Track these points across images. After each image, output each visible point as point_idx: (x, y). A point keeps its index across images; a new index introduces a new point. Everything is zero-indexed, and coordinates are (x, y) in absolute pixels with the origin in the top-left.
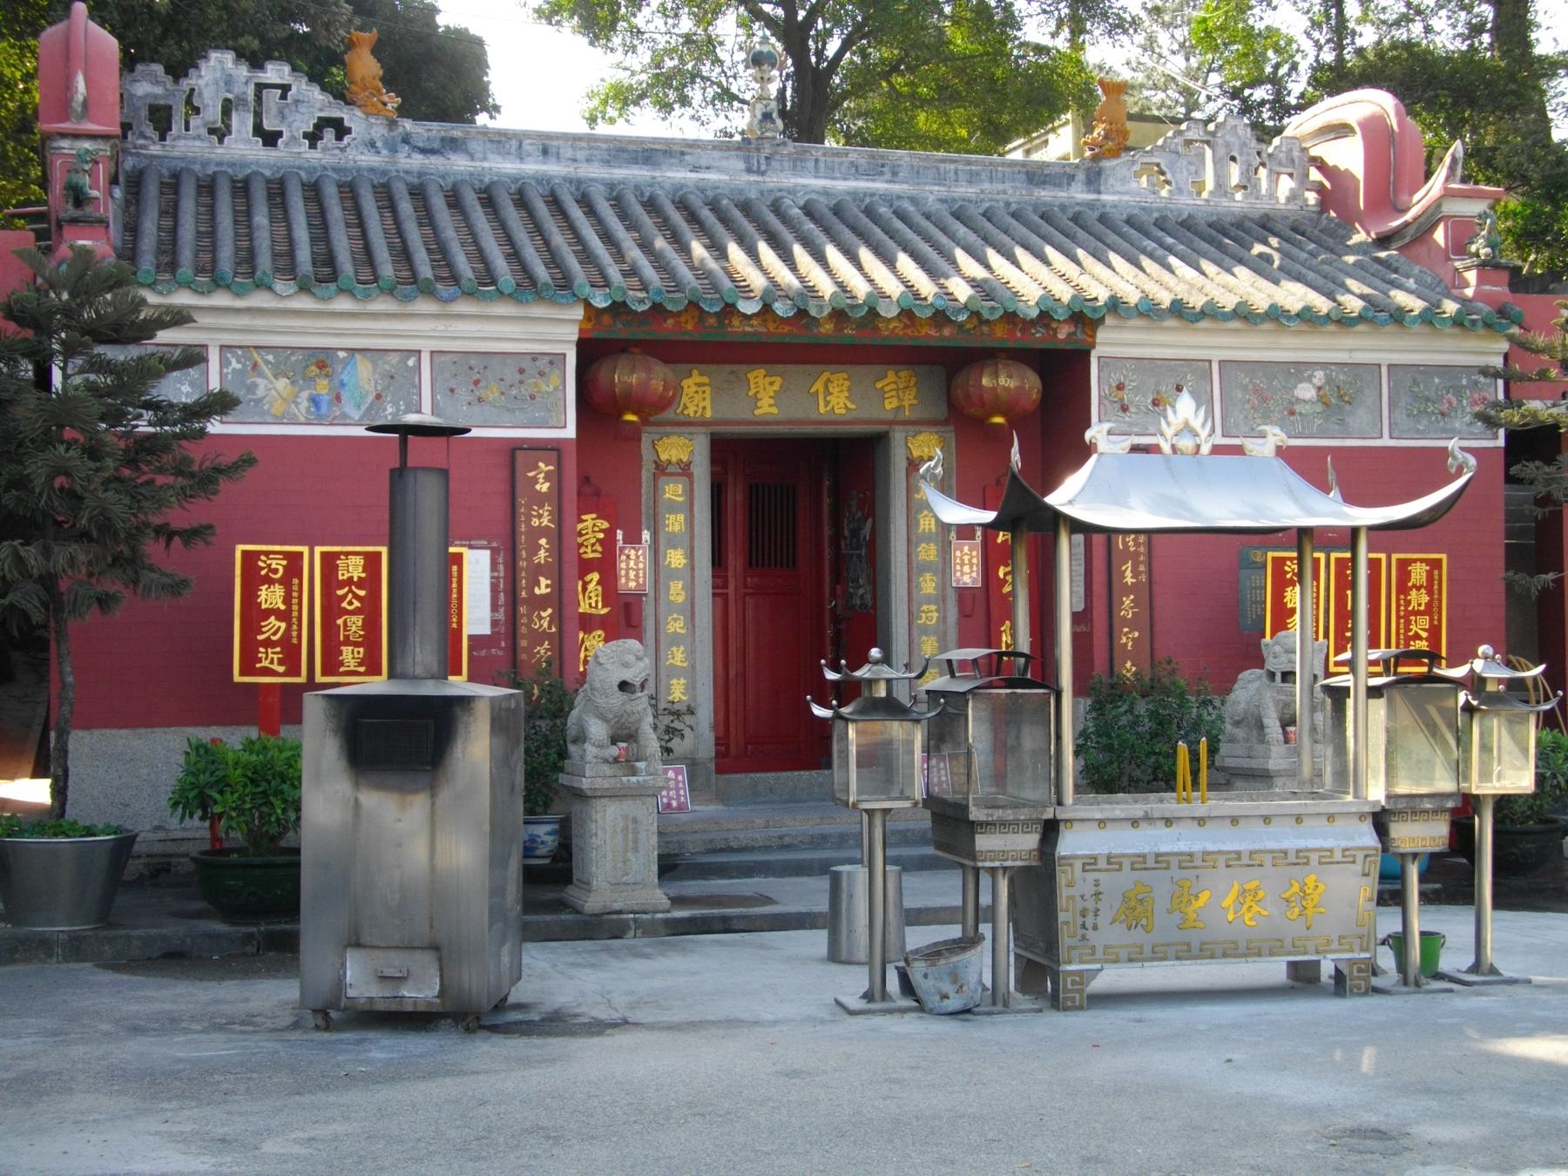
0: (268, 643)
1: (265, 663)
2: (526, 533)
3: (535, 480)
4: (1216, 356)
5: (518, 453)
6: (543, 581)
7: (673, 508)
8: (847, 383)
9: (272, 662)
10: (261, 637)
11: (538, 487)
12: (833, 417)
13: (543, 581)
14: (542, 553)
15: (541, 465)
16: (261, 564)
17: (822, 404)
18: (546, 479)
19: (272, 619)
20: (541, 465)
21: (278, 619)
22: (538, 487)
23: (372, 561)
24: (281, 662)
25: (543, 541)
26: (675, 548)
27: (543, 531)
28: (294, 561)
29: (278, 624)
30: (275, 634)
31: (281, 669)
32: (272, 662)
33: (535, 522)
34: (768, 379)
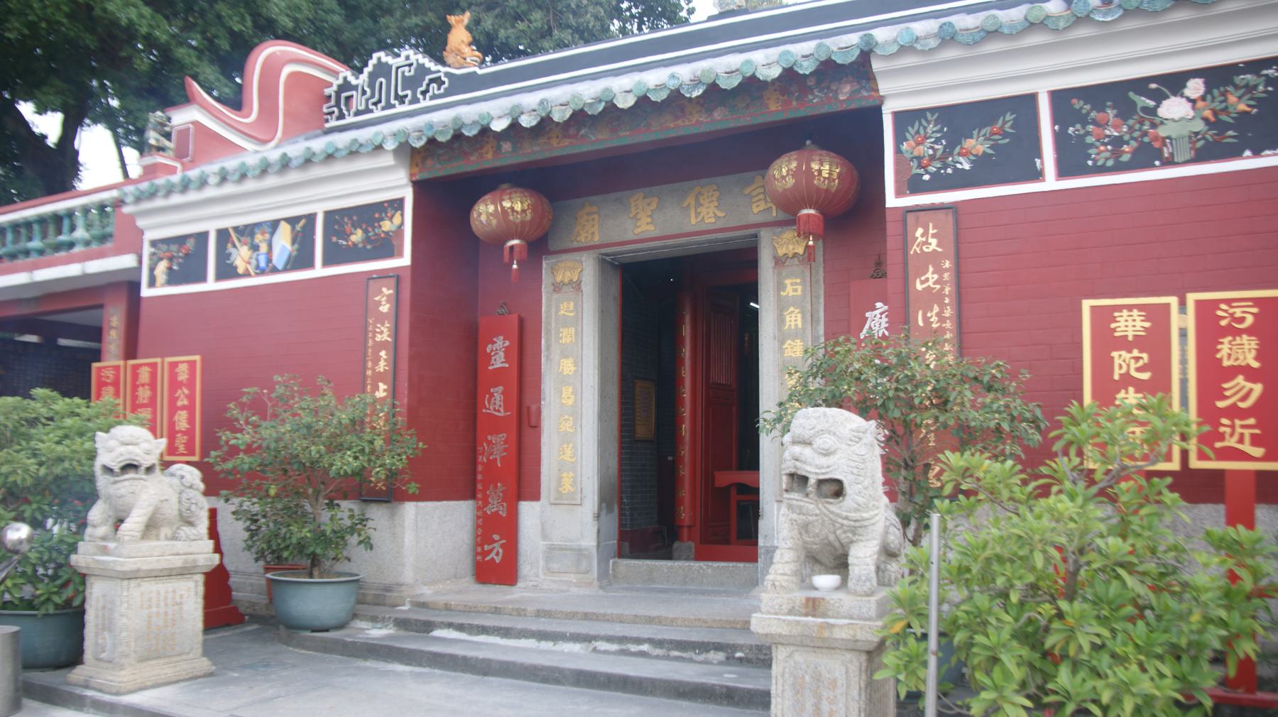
0: (1234, 412)
1: (1231, 442)
2: (373, 347)
3: (379, 303)
4: (212, 227)
5: (371, 282)
6: (382, 386)
7: (565, 323)
8: (717, 194)
9: (1241, 441)
10: (1221, 404)
11: (381, 309)
12: (704, 227)
13: (382, 386)
14: (382, 363)
15: (384, 290)
16: (1220, 313)
17: (693, 215)
18: (387, 301)
19: (1240, 379)
20: (384, 290)
21: (1248, 379)
22: (381, 309)
23: (192, 364)
24: (1255, 441)
25: (383, 354)
26: (566, 357)
27: (383, 345)
28: (1159, 317)
29: (1249, 385)
30: (1244, 399)
31: (1258, 452)
32: (1241, 441)
33: (379, 338)
34: (647, 201)
